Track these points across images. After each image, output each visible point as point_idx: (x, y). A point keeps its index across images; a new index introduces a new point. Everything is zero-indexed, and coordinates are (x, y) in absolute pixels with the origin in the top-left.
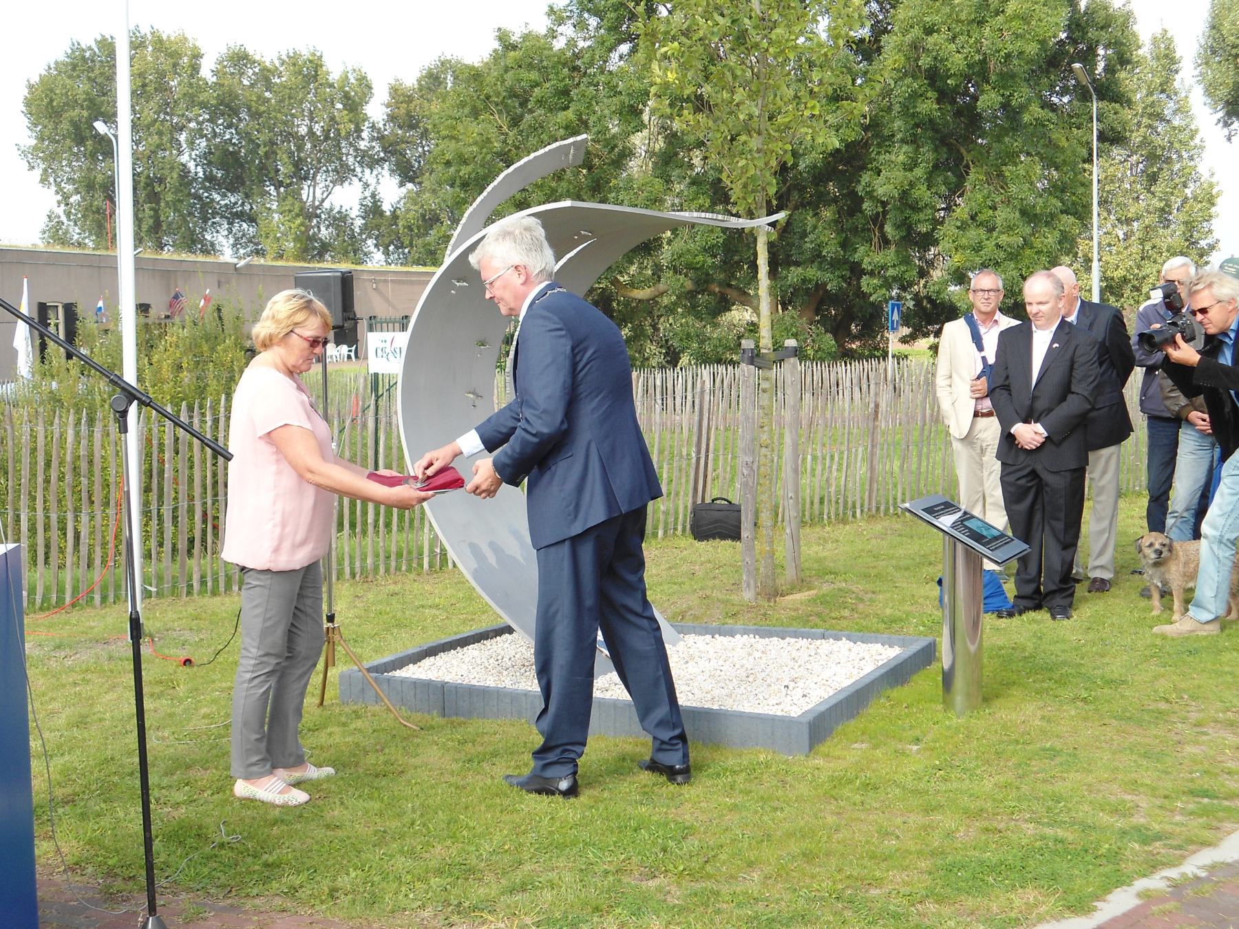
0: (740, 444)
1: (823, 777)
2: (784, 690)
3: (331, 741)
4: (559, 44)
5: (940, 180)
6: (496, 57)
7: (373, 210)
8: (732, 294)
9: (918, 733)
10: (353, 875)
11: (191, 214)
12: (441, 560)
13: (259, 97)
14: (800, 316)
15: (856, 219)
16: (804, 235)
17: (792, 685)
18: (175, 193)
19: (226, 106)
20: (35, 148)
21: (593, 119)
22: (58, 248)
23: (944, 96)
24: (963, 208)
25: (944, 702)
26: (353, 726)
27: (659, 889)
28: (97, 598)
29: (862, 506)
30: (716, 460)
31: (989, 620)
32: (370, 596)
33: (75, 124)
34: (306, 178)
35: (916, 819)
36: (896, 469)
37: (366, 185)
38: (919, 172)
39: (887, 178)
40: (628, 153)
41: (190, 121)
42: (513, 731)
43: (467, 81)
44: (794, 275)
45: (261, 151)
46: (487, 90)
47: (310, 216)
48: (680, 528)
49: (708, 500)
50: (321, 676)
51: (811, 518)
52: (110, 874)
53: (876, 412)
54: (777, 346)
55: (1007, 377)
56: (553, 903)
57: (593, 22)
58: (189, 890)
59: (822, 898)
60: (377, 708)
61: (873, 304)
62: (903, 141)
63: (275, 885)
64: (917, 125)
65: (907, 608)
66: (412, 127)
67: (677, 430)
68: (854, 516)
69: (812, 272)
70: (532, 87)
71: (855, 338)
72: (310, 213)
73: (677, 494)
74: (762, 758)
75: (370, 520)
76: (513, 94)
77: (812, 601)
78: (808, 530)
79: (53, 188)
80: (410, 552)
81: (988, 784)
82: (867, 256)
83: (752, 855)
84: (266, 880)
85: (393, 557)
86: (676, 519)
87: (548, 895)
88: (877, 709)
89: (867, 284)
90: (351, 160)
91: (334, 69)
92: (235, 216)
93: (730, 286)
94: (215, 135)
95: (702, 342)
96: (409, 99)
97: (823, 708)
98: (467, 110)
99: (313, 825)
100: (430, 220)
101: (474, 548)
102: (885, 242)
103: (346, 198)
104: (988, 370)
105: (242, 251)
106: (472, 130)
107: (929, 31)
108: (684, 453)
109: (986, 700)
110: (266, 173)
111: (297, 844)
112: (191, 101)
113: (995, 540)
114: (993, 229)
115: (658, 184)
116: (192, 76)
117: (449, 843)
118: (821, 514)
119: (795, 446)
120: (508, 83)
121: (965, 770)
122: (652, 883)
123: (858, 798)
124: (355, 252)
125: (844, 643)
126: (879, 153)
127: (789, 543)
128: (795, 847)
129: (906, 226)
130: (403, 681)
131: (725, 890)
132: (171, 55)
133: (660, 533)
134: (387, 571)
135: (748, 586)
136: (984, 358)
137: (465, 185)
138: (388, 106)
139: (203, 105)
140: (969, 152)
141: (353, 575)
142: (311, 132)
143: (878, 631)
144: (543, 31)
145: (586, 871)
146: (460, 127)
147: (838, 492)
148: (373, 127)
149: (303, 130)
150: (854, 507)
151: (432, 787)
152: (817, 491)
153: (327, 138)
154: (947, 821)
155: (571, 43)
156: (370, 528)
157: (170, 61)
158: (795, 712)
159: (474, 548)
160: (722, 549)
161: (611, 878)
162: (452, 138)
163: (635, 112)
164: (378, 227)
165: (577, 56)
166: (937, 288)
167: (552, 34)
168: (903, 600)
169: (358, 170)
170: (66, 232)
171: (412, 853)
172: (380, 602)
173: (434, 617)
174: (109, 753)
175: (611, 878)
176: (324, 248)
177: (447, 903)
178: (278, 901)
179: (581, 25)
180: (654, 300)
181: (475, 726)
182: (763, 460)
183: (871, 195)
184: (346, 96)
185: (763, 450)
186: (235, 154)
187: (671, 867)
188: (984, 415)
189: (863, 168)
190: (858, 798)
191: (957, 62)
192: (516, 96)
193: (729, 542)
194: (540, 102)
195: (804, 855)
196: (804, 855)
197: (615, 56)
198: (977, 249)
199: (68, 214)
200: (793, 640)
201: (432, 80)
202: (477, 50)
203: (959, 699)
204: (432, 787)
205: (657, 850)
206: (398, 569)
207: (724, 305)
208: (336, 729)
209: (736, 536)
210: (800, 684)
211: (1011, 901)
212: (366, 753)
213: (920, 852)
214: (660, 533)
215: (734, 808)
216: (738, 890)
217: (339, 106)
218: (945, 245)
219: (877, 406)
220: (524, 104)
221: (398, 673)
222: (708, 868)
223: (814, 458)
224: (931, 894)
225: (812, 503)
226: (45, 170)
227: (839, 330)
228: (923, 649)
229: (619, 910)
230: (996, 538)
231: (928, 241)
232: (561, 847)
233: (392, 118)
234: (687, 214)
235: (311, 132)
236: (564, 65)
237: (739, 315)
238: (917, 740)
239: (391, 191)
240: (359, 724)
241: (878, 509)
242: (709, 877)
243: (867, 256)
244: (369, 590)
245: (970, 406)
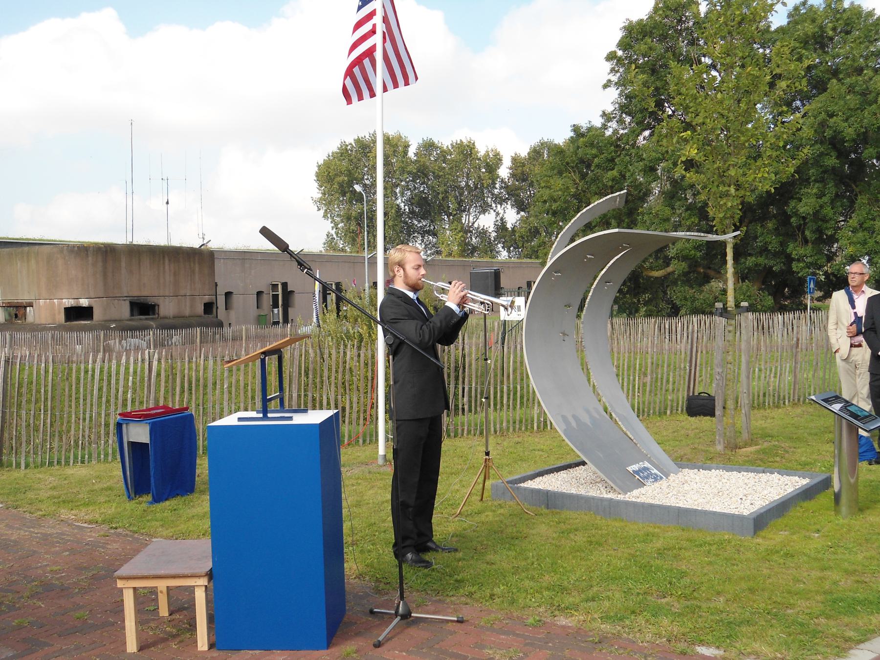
0: (715, 361)
1: (762, 549)
2: (740, 501)
3: (487, 520)
4: (609, 133)
5: (839, 204)
6: (572, 140)
7: (501, 227)
8: (711, 273)
9: (818, 527)
10: (502, 588)
11: (401, 232)
12: (544, 425)
13: (439, 167)
14: (753, 286)
15: (789, 230)
16: (756, 237)
17: (744, 498)
18: (393, 221)
19: (421, 172)
20: (321, 199)
21: (628, 174)
22: (331, 253)
23: (842, 154)
24: (854, 222)
25: (835, 510)
26: (499, 512)
27: (667, 604)
28: (361, 441)
29: (789, 398)
30: (701, 370)
31: (864, 465)
32: (505, 444)
33: (341, 185)
34: (464, 211)
35: (815, 574)
36: (810, 376)
37: (498, 214)
38: (825, 199)
39: (805, 204)
40: (648, 193)
41: (402, 181)
42: (586, 518)
43: (556, 155)
44: (750, 261)
45: (440, 196)
46: (568, 160)
47: (466, 232)
48: (680, 409)
49: (696, 394)
50: (481, 485)
51: (758, 404)
52: (378, 580)
53: (798, 343)
54: (737, 306)
55: (873, 324)
56: (609, 608)
57: (628, 119)
58: (418, 591)
59: (759, 613)
60: (511, 503)
61: (800, 278)
62: (816, 181)
63: (462, 591)
64: (824, 172)
65: (814, 457)
66: (524, 180)
67: (678, 353)
68: (784, 403)
69: (761, 260)
70: (594, 158)
71: (786, 298)
72: (467, 230)
73: (678, 390)
74: (726, 537)
75: (505, 402)
76: (582, 161)
77: (758, 452)
78: (756, 411)
79: (330, 220)
80: (526, 420)
81: (860, 557)
82: (795, 249)
83: (720, 588)
84: (456, 589)
85: (517, 422)
86: (678, 404)
87: (607, 604)
88: (795, 513)
89: (795, 266)
90: (489, 200)
91: (481, 149)
92: (424, 233)
93: (710, 268)
94: (415, 188)
95: (694, 301)
96: (523, 165)
97: (762, 511)
98: (555, 172)
99: (480, 562)
100: (535, 232)
101: (564, 418)
102: (806, 241)
103: (487, 222)
104: (858, 319)
105: (429, 252)
106: (558, 183)
107: (831, 116)
108: (682, 366)
109: (861, 510)
110: (443, 209)
111: (472, 571)
112: (403, 171)
113: (865, 418)
114: (873, 232)
115: (668, 211)
116: (404, 157)
117: (552, 574)
118: (764, 402)
119: (748, 363)
120: (580, 155)
121: (846, 549)
122: (664, 601)
123: (782, 561)
124: (491, 251)
125: (776, 476)
126: (801, 189)
127: (744, 418)
128: (744, 585)
129: (819, 231)
130: (525, 489)
131: (704, 606)
132: (393, 146)
133: (668, 412)
134: (514, 430)
135: (719, 442)
136: (855, 313)
137: (554, 214)
138: (511, 168)
139: (409, 173)
140: (857, 186)
141: (495, 432)
142: (467, 185)
143: (797, 469)
144: (599, 125)
145: (627, 592)
146: (552, 181)
147: (774, 390)
148: (502, 181)
149: (463, 184)
150: (784, 399)
151: (543, 545)
152: (762, 388)
153: (476, 188)
154: (835, 575)
155: (615, 132)
156: (505, 407)
157: (392, 149)
158: (746, 513)
159: (564, 418)
160: (704, 422)
161: (641, 597)
162: (547, 187)
163: (653, 169)
164: (504, 237)
165: (619, 139)
166: (837, 267)
167: (605, 127)
168: (813, 453)
169: (494, 205)
170: (336, 244)
171: (533, 578)
172: (511, 447)
173: (541, 456)
174: (373, 521)
175: (641, 597)
176: (474, 249)
177: (552, 605)
178: (463, 599)
179: (621, 121)
180: (666, 277)
181: (566, 514)
182: (729, 371)
183: (796, 214)
184: (487, 164)
185: (729, 366)
186: (426, 199)
187: (674, 592)
188: (856, 346)
189: (792, 198)
190: (782, 561)
191: (849, 132)
192: (584, 162)
193: (708, 418)
194: (598, 166)
195: (750, 589)
196: (750, 589)
197: (641, 138)
198: (864, 243)
199: (337, 234)
200: (745, 473)
201: (536, 153)
202: (561, 136)
203: (844, 509)
204: (543, 545)
205: (667, 583)
206: (520, 429)
207: (707, 279)
208: (490, 513)
209: (713, 415)
210: (750, 497)
211: (870, 620)
212: (507, 526)
213: (817, 592)
214: (668, 412)
215: (710, 563)
216: (711, 606)
217: (484, 170)
218: (843, 242)
219: (798, 340)
220: (588, 166)
221: (522, 485)
222: (695, 594)
223: (760, 370)
224: (823, 614)
225: (759, 396)
226: (326, 210)
227: (777, 293)
228: (823, 480)
229: (645, 613)
230: (866, 417)
231: (832, 239)
232: (614, 579)
233: (513, 175)
234: (681, 233)
235: (467, 185)
236: (611, 145)
237: (716, 285)
238: (818, 531)
239: (512, 216)
240: (501, 511)
241: (799, 400)
242: (695, 598)
243: (795, 249)
244: (504, 440)
245: (848, 342)
